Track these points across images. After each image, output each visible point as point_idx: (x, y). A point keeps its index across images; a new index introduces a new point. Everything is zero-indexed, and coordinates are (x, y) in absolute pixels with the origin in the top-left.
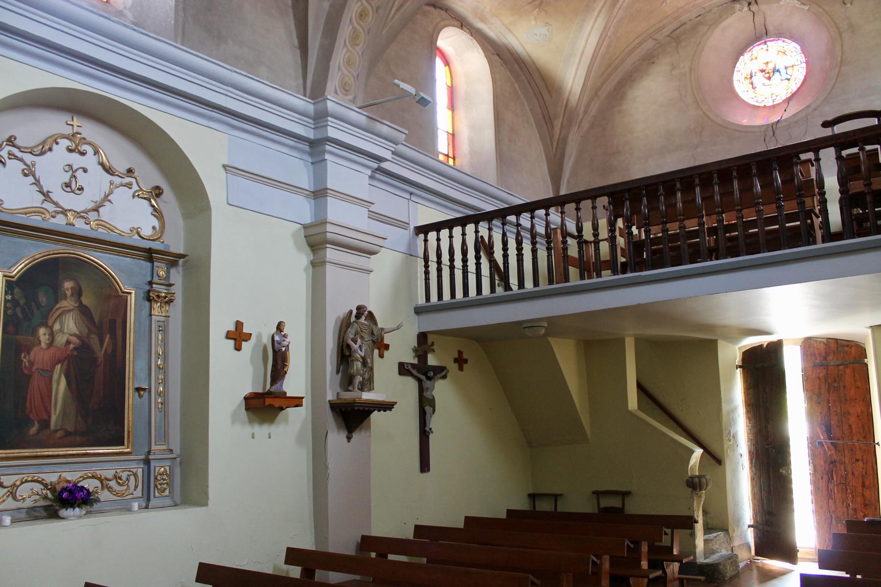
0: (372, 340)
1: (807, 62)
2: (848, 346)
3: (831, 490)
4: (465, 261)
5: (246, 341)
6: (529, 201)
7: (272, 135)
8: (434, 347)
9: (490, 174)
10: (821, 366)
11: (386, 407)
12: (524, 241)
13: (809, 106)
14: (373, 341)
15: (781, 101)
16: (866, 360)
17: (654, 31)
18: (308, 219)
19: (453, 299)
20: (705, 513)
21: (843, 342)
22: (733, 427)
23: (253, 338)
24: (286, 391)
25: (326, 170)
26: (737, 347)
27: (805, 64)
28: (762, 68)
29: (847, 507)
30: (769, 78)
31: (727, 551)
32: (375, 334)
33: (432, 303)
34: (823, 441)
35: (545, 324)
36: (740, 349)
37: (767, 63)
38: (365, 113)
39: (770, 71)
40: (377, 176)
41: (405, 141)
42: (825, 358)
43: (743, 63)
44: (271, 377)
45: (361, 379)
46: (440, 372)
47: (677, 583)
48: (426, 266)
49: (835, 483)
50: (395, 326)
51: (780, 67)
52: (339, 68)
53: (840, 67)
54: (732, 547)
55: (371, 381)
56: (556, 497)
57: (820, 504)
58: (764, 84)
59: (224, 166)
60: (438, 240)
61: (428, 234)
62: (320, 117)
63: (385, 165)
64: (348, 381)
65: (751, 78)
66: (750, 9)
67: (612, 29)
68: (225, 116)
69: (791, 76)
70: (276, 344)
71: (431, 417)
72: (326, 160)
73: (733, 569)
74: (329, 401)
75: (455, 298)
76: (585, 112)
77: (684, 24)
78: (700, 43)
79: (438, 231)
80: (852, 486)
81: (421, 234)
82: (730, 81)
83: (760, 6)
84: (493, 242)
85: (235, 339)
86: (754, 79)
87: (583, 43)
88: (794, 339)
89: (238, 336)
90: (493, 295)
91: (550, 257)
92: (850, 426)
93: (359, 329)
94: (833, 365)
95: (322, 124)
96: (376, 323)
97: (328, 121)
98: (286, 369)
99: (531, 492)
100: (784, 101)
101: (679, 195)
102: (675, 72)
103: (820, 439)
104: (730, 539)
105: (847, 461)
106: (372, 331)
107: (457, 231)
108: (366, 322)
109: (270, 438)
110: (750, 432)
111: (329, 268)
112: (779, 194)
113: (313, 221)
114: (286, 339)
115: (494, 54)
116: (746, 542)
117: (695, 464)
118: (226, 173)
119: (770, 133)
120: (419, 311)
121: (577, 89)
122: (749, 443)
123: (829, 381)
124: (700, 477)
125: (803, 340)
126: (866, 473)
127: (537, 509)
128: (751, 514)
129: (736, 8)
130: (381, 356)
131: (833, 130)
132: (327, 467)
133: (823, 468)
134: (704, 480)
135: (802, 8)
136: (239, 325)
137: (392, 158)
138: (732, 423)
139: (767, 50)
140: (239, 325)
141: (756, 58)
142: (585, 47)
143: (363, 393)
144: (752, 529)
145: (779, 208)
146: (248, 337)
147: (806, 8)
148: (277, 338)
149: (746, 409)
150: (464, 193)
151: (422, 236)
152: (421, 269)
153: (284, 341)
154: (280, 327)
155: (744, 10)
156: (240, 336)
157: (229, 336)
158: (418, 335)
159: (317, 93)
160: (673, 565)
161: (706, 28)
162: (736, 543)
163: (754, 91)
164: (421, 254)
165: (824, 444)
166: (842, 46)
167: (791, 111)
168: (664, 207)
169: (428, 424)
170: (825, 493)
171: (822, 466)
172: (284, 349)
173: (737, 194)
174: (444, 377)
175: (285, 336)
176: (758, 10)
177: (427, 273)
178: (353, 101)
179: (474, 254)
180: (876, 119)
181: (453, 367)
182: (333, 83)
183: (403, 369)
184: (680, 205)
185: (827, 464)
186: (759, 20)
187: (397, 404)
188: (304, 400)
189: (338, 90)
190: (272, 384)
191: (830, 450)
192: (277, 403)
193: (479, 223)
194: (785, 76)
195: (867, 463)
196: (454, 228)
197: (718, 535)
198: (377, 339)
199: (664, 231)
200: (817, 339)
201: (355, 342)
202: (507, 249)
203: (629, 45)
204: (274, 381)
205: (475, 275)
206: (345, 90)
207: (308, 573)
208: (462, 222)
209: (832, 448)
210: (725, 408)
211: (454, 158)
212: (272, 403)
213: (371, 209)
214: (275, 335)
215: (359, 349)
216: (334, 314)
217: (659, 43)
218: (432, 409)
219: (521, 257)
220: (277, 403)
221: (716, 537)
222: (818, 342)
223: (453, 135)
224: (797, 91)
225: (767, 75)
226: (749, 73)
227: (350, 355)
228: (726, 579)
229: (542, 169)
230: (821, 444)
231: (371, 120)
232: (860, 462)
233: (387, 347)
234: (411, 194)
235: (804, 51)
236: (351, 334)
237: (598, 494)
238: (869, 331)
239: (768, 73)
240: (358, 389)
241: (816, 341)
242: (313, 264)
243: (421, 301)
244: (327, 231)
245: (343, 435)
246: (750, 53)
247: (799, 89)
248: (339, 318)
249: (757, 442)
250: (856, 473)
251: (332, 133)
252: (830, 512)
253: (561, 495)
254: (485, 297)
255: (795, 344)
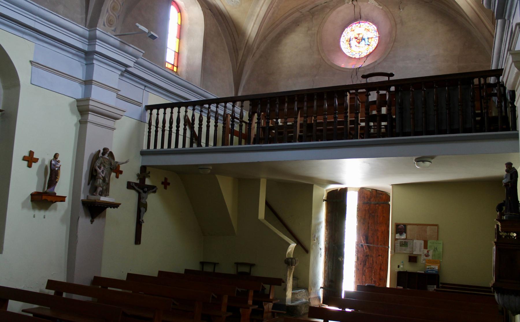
0: (110, 168)
1: (379, 37)
2: (381, 194)
3: (364, 270)
4: (171, 127)
5: (35, 162)
6: (219, 97)
7: (62, 46)
8: (150, 175)
9: (197, 79)
10: (367, 204)
11: (115, 206)
12: (211, 118)
13: (376, 62)
14: (111, 168)
15: (363, 56)
16: (389, 202)
17: (300, 8)
18: (80, 96)
19: (148, 149)
20: (294, 278)
21: (380, 192)
22: (317, 233)
23: (39, 162)
24: (56, 192)
25: (93, 70)
26: (325, 189)
27: (378, 38)
28: (356, 36)
29: (371, 280)
30: (359, 43)
31: (306, 300)
32: (113, 165)
33: (179, 148)
34: (363, 244)
35: (211, 168)
36: (326, 190)
37: (359, 34)
38: (119, 39)
39: (360, 39)
40: (125, 75)
41: (142, 56)
42: (370, 200)
43: (347, 32)
44: (48, 184)
45: (101, 189)
46: (152, 189)
47: (270, 314)
48: (150, 128)
49: (367, 267)
50: (125, 161)
51: (365, 37)
52: (107, 11)
53: (394, 43)
54: (309, 298)
55: (107, 191)
56: (215, 264)
57: (358, 278)
58: (356, 46)
59: (31, 62)
60: (158, 114)
61: (153, 110)
62: (92, 39)
63: (129, 69)
64: (93, 190)
65: (350, 41)
66: (353, 3)
67: (275, 3)
68: (33, 32)
69: (370, 43)
70: (52, 166)
71: (144, 213)
72: (94, 63)
73: (306, 309)
74: (82, 200)
75: (170, 148)
76: (258, 48)
77: (318, 6)
78: (324, 17)
79: (158, 109)
80: (375, 269)
81: (149, 110)
82: (339, 42)
83: (358, 2)
84: (194, 118)
85: (28, 161)
86: (351, 42)
87: (258, 9)
88: (355, 188)
89: (30, 159)
90: (191, 148)
91: (216, 131)
92: (378, 237)
93: (103, 161)
94: (373, 204)
95: (92, 43)
96: (114, 158)
97: (96, 42)
98: (57, 180)
99: (202, 261)
100: (365, 56)
101: (286, 105)
102: (309, 32)
103: (362, 243)
104: (309, 294)
105: (374, 256)
106: (111, 163)
107: (169, 110)
108: (108, 158)
109: (44, 218)
110: (327, 237)
111: (89, 125)
112: (336, 110)
113: (83, 97)
114: (59, 164)
115: (207, 9)
116: (318, 296)
117: (291, 252)
118: (32, 66)
119: (354, 74)
120: (143, 153)
121: (253, 35)
122: (326, 243)
123: (370, 212)
124: (292, 259)
125: (360, 189)
126: (383, 263)
127: (205, 270)
128: (323, 281)
129: (346, 1)
130: (117, 177)
131: (367, 81)
132: (77, 237)
133: (362, 259)
134: (294, 260)
135: (379, 8)
136: (31, 153)
137: (134, 65)
138: (317, 231)
139: (360, 27)
140: (31, 153)
141: (354, 31)
142: (260, 12)
143: (101, 197)
144: (323, 289)
145: (335, 118)
146: (36, 160)
147: (381, 8)
148: (53, 162)
149: (326, 224)
150: (176, 88)
151: (149, 111)
152: (146, 130)
153: (57, 164)
154: (56, 156)
155: (349, 3)
156: (31, 159)
157: (25, 158)
158: (141, 167)
159: (92, 25)
160: (269, 304)
161: (328, 10)
162: (312, 296)
163: (350, 48)
164: (147, 121)
165: (364, 246)
166: (396, 32)
167: (367, 63)
168: (278, 110)
169: (141, 218)
170: (361, 272)
171: (361, 258)
172: (57, 169)
173: (315, 108)
174: (155, 192)
175: (58, 162)
176: (357, 5)
177: (149, 132)
178: (115, 31)
179: (176, 124)
180: (388, 77)
181: (160, 187)
182: (103, 19)
183: (130, 186)
184: (286, 110)
185: (364, 257)
186: (357, 10)
187: (121, 205)
188: (66, 198)
189: (106, 24)
190: (48, 188)
191: (366, 249)
192: (49, 199)
193: (188, 107)
194: (367, 43)
195: (383, 257)
196: (167, 109)
197: (301, 291)
198: (113, 168)
199: (325, 119)
200: (367, 189)
201: (100, 168)
202: (202, 124)
203: (285, 13)
204: (49, 187)
205: (183, 136)
206: (110, 24)
207: (59, 293)
208: (179, 105)
209: (367, 248)
210: (313, 222)
211: (177, 67)
212: (47, 199)
213: (118, 93)
214: (52, 161)
215: (101, 173)
216: (90, 151)
217: (303, 14)
218: (145, 209)
219: (200, 129)
220: (49, 199)
221: (300, 292)
222: (367, 191)
223: (178, 53)
224: (372, 52)
225: (358, 41)
226: (349, 38)
227: (96, 175)
228: (301, 314)
229: (230, 79)
230: (362, 245)
231: (122, 44)
232: (380, 256)
233: (121, 172)
234: (145, 86)
235: (378, 30)
236: (98, 164)
237: (237, 264)
238: (391, 187)
239: (359, 40)
240: (99, 194)
241: (366, 190)
242: (80, 122)
243: (145, 148)
244: (90, 104)
245: (88, 220)
246: (351, 27)
247: (373, 51)
248: (92, 153)
249: (329, 242)
250: (378, 262)
251: (98, 49)
252: (362, 282)
253: (218, 263)
254: (179, 149)
255: (356, 191)
